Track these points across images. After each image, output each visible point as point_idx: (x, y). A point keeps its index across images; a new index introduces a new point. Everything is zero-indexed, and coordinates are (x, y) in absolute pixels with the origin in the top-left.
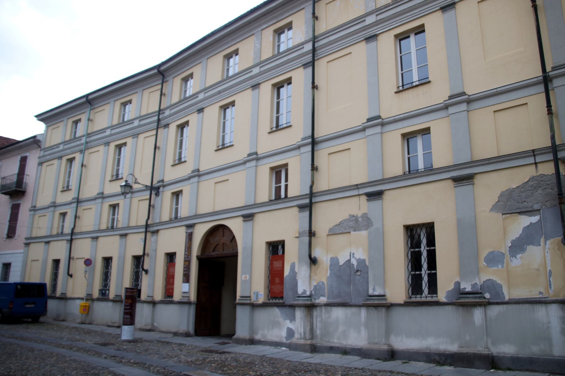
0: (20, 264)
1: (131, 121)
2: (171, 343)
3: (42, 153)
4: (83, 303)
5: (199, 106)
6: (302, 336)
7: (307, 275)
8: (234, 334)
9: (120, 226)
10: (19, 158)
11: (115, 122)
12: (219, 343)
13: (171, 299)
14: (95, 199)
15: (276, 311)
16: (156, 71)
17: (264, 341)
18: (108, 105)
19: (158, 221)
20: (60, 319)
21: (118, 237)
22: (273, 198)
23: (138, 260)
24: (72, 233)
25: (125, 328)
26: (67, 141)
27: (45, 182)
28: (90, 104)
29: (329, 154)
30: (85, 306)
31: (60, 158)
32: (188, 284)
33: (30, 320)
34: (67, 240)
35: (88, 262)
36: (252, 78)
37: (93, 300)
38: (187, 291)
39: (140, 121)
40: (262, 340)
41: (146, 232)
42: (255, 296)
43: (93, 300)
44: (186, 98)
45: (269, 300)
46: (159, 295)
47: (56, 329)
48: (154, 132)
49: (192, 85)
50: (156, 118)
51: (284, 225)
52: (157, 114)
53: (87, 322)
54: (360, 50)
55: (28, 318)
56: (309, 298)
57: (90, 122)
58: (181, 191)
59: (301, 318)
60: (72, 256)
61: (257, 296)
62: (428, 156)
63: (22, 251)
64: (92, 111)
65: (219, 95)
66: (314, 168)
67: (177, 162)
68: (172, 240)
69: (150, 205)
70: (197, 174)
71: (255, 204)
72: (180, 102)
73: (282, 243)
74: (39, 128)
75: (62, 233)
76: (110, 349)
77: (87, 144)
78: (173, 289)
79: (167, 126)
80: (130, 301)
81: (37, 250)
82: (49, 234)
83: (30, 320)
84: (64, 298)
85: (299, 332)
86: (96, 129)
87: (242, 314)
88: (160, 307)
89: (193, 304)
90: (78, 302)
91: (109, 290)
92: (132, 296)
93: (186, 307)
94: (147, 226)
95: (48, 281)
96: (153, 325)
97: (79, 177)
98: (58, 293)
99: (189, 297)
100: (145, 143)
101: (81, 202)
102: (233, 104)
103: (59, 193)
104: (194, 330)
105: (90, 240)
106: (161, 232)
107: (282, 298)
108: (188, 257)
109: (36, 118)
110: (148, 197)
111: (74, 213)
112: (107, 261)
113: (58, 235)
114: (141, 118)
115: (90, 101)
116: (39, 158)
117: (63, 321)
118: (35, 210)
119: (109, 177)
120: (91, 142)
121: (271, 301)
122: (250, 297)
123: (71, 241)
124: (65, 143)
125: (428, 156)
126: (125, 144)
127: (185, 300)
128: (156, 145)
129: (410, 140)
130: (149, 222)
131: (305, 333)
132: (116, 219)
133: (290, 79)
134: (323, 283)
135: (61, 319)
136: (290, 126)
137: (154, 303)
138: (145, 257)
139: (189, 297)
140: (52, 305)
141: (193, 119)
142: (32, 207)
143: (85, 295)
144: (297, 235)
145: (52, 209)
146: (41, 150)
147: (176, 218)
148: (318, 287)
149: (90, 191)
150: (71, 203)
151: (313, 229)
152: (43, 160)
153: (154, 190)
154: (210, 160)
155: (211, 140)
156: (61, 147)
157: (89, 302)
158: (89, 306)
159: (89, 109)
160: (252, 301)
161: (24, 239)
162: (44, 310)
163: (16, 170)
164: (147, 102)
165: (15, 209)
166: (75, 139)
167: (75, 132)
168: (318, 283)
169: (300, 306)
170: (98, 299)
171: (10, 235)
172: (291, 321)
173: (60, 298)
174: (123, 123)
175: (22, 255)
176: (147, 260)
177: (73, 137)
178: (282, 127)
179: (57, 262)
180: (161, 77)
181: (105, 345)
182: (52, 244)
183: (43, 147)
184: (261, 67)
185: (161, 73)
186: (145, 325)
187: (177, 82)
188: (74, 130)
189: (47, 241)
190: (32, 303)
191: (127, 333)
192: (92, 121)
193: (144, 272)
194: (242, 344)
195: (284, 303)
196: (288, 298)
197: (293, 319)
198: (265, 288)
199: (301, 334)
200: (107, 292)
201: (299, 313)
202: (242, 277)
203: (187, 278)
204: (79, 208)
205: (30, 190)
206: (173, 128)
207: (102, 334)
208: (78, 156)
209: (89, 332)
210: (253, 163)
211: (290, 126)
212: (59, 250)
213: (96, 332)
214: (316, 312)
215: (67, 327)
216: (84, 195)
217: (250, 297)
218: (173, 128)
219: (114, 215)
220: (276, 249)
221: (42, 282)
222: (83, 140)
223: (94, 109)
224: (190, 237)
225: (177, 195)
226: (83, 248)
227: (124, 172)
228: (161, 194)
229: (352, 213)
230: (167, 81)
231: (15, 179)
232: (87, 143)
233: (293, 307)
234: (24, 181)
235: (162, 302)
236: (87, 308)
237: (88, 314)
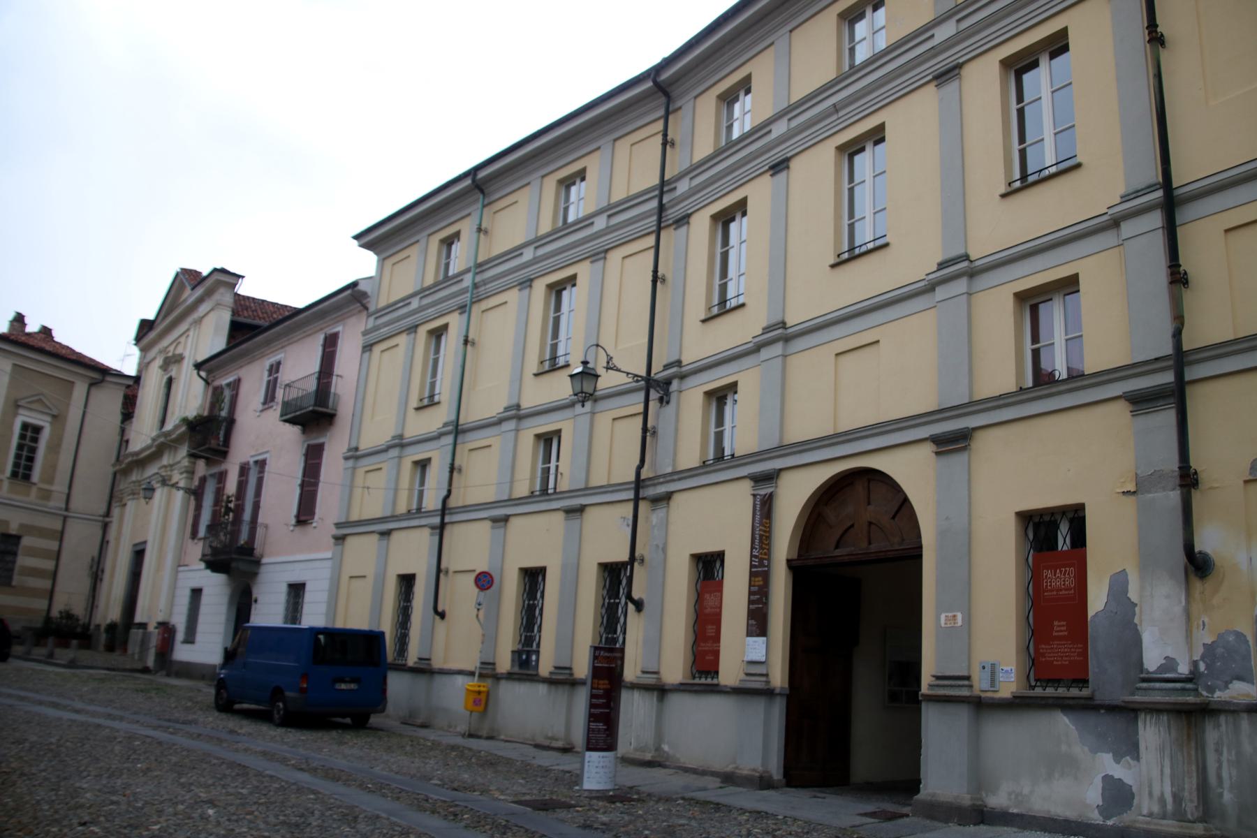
0: (325, 585)
1: (586, 221)
2: (729, 809)
3: (371, 323)
4: (472, 683)
6: (1170, 807)
7: (1178, 609)
8: (917, 791)
9: (564, 485)
10: (320, 338)
11: (546, 227)
12: (872, 815)
13: (709, 681)
14: (499, 422)
15: (1063, 722)
16: (649, 84)
17: (1020, 816)
19: (669, 470)
20: (416, 721)
21: (560, 516)
22: (1030, 383)
23: (615, 577)
24: (444, 510)
25: (593, 757)
26: (429, 288)
27: (379, 390)
28: (482, 192)
29: (1227, 231)
30: (479, 693)
31: (413, 329)
33: (348, 720)
34: (433, 528)
35: (484, 581)
36: (935, 52)
37: (497, 678)
38: (763, 659)
39: (609, 216)
40: (1015, 811)
41: (636, 500)
42: (987, 675)
43: (497, 678)
44: (731, 144)
45: (1033, 688)
46: (674, 669)
47: (408, 748)
48: (651, 241)
50: (654, 204)
51: (1088, 460)
52: (657, 193)
53: (484, 733)
54: (513, 296)
55: (344, 716)
56: (1189, 686)
57: (482, 235)
58: (733, 387)
59: (1162, 749)
60: (443, 566)
61: (993, 673)
62: (1074, 341)
63: (329, 555)
64: (486, 210)
65: (835, 117)
66: (1178, 278)
67: (715, 311)
68: (715, 519)
69: (645, 429)
70: (780, 335)
71: (971, 403)
72: (718, 154)
73: (1076, 516)
74: (364, 265)
75: (419, 509)
76: (563, 821)
77: (475, 291)
78: (717, 654)
79: (684, 220)
80: (604, 684)
81: (362, 550)
82: (388, 514)
83: (348, 720)
84: (424, 670)
85: (1156, 793)
86: (496, 251)
87: (941, 736)
88: (677, 702)
89: (780, 694)
90: (460, 680)
91: (538, 653)
92: (610, 669)
93: (759, 705)
94: (638, 483)
95: (387, 626)
96: (658, 749)
97: (459, 370)
99: (767, 675)
100: (627, 273)
101: (465, 431)
102: (877, 136)
103: (411, 412)
104: (782, 770)
105: (488, 524)
107: (1083, 682)
108: (761, 565)
109: (356, 242)
110: (640, 408)
111: (449, 460)
112: (533, 578)
113: (409, 515)
114: (611, 210)
115: (482, 185)
116: (365, 333)
117: (424, 726)
118: (357, 458)
119: (532, 366)
120: (485, 282)
121: (1038, 691)
122: (968, 678)
123: (442, 527)
124: (423, 292)
125: (1074, 341)
126: (572, 280)
127: (757, 684)
128: (655, 271)
129: (1041, 306)
130: (645, 474)
131: (1177, 798)
132: (552, 471)
133: (881, 128)
134: (1240, 636)
135: (419, 721)
136: (886, 245)
137: (661, 691)
138: (636, 564)
139: (767, 675)
140: (397, 685)
141: (760, 193)
142: (350, 450)
143: (478, 665)
144: (1132, 488)
145: (394, 453)
146: (369, 316)
147: (720, 457)
148: (1220, 651)
149: (486, 401)
153: (657, 387)
154: (816, 292)
155: (815, 240)
156: (415, 303)
157: (489, 682)
158: (488, 693)
159: (480, 205)
160: (976, 692)
161: (333, 527)
162: (378, 699)
163: (314, 365)
164: (630, 166)
165: (313, 457)
166: (447, 279)
167: (447, 265)
168: (1220, 636)
169: (1155, 710)
170: (510, 676)
171: (302, 518)
172: (1118, 758)
173: (415, 671)
175: (329, 564)
176: (640, 574)
177: (441, 277)
178: (864, 249)
179: (407, 581)
180: (663, 100)
181: (544, 806)
182: (396, 537)
183: (372, 308)
184: (958, 21)
185: (660, 90)
186: (636, 750)
187: (707, 106)
188: (444, 261)
189: (384, 529)
190: (352, 681)
191: (596, 771)
192: (486, 232)
193: (631, 607)
194: (946, 821)
195: (1091, 698)
196: (1106, 679)
197: (1130, 749)
198: (1018, 653)
199: (1162, 800)
200: (534, 658)
201: (1151, 734)
202: (938, 619)
203: (758, 623)
204: (459, 448)
205: (345, 411)
206: (701, 224)
207: (525, 770)
208: (455, 322)
209: (491, 763)
210: (961, 286)
211: (886, 245)
212: (411, 550)
213: (509, 762)
214: (1213, 733)
215: (436, 745)
216: (471, 415)
217: (968, 678)
218: (701, 224)
219: (547, 459)
220: (1053, 536)
221: (375, 629)
222: (468, 281)
223: (490, 204)
224: (765, 509)
225: (720, 397)
226: (471, 546)
227: (573, 351)
229: (199, 556)
230: (680, 108)
231: (312, 386)
232: (476, 286)
233: (1130, 712)
234: (333, 390)
235: (682, 688)
236: (483, 697)
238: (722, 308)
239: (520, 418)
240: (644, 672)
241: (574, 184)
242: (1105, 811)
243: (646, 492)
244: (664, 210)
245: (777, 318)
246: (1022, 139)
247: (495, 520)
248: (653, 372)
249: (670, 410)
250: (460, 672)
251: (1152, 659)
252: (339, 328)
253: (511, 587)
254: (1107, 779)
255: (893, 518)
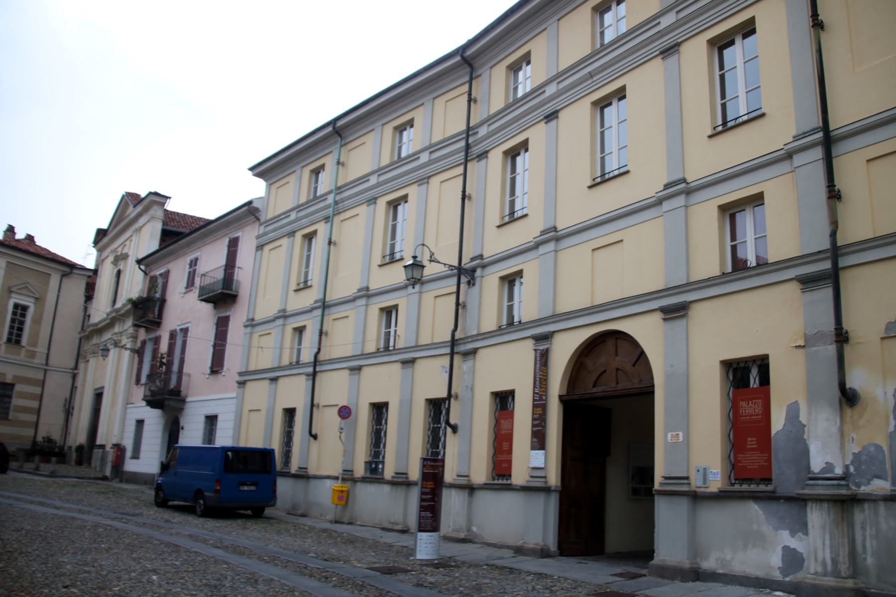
1: (415, 156)
3: (262, 230)
5: (549, 108)
9: (400, 344)
14: (354, 299)
16: (458, 58)
18: (371, 135)
19: (475, 332)
20: (297, 512)
21: (398, 366)
23: (437, 408)
24: (316, 362)
28: (340, 136)
32: (542, 452)
34: (308, 375)
35: (345, 412)
37: (354, 481)
40: (721, 571)
41: (452, 354)
43: (354, 481)
46: (480, 473)
48: (461, 170)
49: (529, 74)
50: (462, 144)
51: (770, 323)
52: (464, 135)
53: (346, 520)
60: (315, 402)
61: (705, 475)
64: (343, 149)
65: (590, 81)
68: (508, 367)
69: (458, 304)
80: (430, 484)
84: (303, 476)
90: (328, 483)
91: (383, 463)
94: (454, 342)
95: (276, 445)
96: (469, 530)
98: (294, 468)
99: (545, 477)
100: (444, 192)
101: (329, 306)
105: (347, 372)
106: (481, 353)
107: (768, 480)
110: (454, 289)
111: (318, 327)
112: (379, 410)
113: (291, 366)
114: (432, 148)
115: (339, 131)
116: (258, 237)
117: (303, 516)
119: (377, 259)
120: (343, 200)
121: (737, 487)
122: (687, 478)
123: (314, 375)
131: (835, 562)
134: (878, 447)
136: (628, 172)
140: (283, 486)
144: (802, 343)
145: (280, 322)
146: (260, 225)
149: (344, 286)
150: (312, 310)
151: (846, 326)
152: (263, 240)
153: (466, 273)
157: (347, 486)
162: (271, 497)
164: (445, 117)
166: (316, 198)
170: (364, 480)
174: (400, 161)
176: (454, 405)
177: (311, 197)
178: (611, 175)
179: (290, 413)
182: (281, 382)
183: (263, 219)
187: (499, 73)
193: (449, 430)
197: (801, 527)
201: (816, 517)
203: (539, 440)
206: (496, 157)
208: (322, 229)
210: (680, 201)
211: (628, 172)
212: (292, 390)
218: (496, 157)
219: (388, 325)
221: (268, 447)
222: (330, 199)
224: (543, 359)
228: (478, 281)
232: (336, 203)
233: (801, 501)
236: (345, 494)
237: (346, 505)
238: (512, 217)
239: (369, 297)
240: (459, 476)
241: (405, 129)
242: (784, 571)
243: (460, 348)
244: (470, 149)
245: (550, 224)
246: (723, 96)
247: (352, 369)
248: (463, 263)
249: (475, 290)
250: (328, 477)
251: (817, 464)
252: (239, 234)
253: (364, 416)
254: (786, 549)
255: (634, 365)
